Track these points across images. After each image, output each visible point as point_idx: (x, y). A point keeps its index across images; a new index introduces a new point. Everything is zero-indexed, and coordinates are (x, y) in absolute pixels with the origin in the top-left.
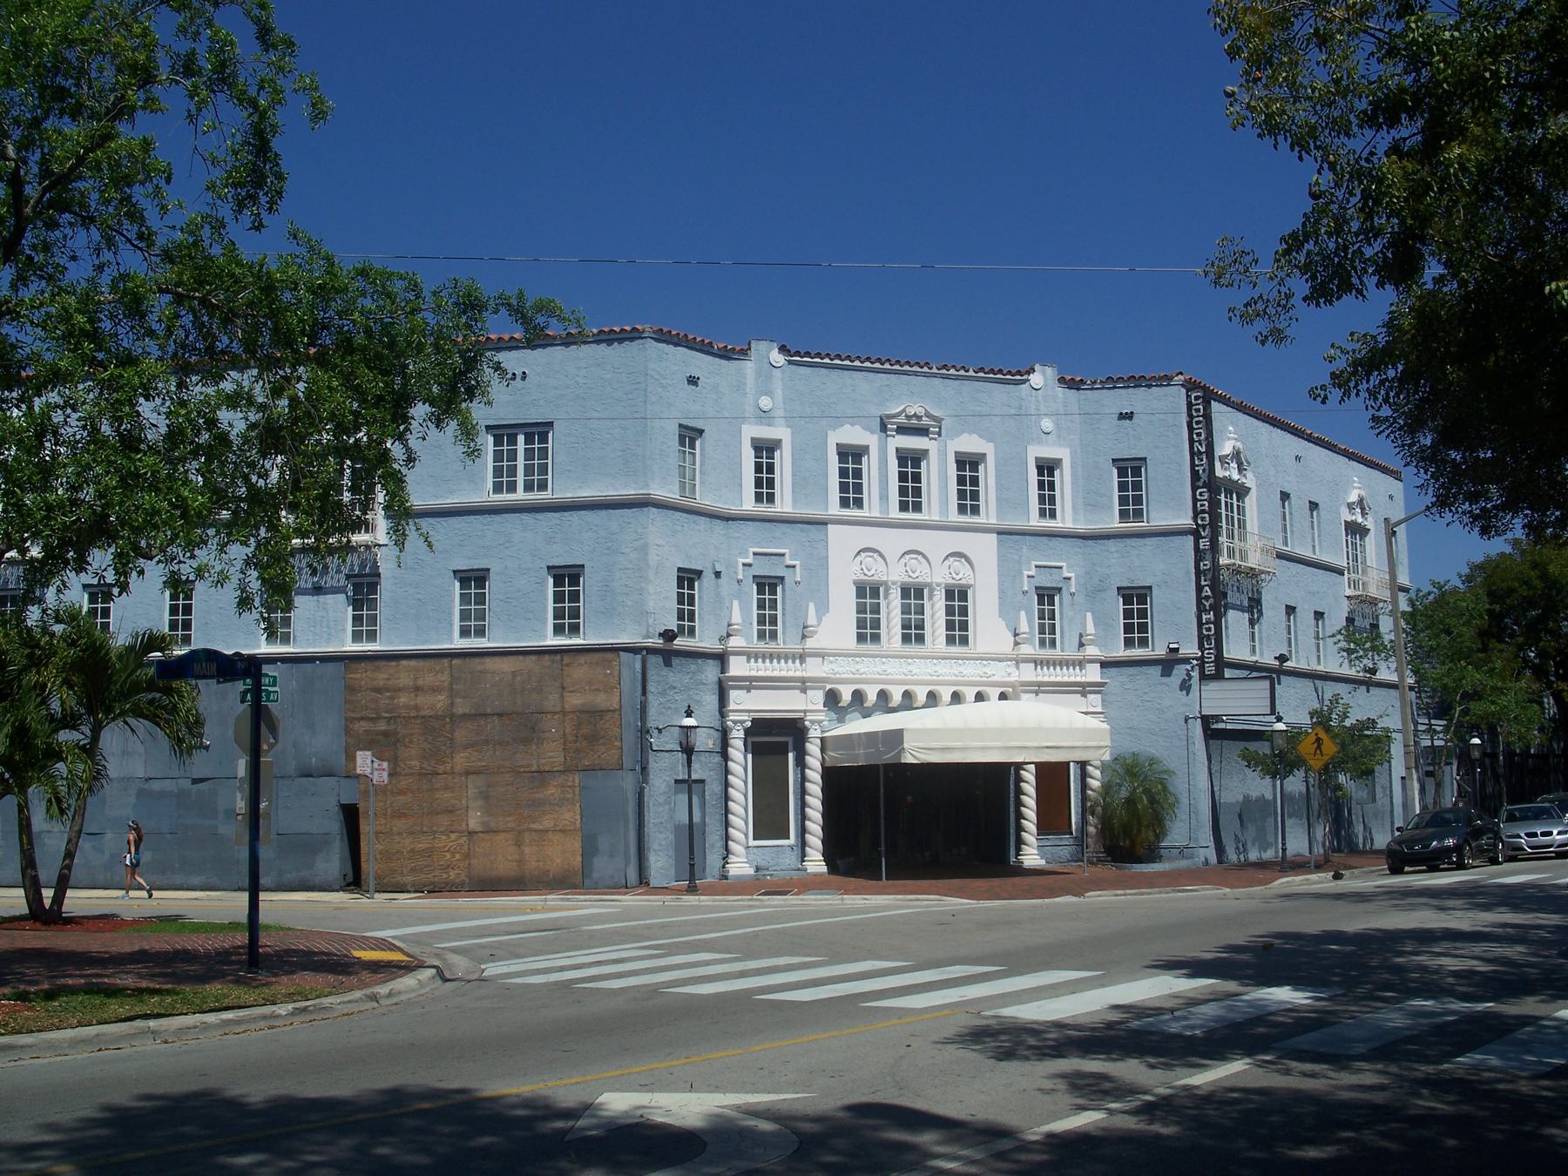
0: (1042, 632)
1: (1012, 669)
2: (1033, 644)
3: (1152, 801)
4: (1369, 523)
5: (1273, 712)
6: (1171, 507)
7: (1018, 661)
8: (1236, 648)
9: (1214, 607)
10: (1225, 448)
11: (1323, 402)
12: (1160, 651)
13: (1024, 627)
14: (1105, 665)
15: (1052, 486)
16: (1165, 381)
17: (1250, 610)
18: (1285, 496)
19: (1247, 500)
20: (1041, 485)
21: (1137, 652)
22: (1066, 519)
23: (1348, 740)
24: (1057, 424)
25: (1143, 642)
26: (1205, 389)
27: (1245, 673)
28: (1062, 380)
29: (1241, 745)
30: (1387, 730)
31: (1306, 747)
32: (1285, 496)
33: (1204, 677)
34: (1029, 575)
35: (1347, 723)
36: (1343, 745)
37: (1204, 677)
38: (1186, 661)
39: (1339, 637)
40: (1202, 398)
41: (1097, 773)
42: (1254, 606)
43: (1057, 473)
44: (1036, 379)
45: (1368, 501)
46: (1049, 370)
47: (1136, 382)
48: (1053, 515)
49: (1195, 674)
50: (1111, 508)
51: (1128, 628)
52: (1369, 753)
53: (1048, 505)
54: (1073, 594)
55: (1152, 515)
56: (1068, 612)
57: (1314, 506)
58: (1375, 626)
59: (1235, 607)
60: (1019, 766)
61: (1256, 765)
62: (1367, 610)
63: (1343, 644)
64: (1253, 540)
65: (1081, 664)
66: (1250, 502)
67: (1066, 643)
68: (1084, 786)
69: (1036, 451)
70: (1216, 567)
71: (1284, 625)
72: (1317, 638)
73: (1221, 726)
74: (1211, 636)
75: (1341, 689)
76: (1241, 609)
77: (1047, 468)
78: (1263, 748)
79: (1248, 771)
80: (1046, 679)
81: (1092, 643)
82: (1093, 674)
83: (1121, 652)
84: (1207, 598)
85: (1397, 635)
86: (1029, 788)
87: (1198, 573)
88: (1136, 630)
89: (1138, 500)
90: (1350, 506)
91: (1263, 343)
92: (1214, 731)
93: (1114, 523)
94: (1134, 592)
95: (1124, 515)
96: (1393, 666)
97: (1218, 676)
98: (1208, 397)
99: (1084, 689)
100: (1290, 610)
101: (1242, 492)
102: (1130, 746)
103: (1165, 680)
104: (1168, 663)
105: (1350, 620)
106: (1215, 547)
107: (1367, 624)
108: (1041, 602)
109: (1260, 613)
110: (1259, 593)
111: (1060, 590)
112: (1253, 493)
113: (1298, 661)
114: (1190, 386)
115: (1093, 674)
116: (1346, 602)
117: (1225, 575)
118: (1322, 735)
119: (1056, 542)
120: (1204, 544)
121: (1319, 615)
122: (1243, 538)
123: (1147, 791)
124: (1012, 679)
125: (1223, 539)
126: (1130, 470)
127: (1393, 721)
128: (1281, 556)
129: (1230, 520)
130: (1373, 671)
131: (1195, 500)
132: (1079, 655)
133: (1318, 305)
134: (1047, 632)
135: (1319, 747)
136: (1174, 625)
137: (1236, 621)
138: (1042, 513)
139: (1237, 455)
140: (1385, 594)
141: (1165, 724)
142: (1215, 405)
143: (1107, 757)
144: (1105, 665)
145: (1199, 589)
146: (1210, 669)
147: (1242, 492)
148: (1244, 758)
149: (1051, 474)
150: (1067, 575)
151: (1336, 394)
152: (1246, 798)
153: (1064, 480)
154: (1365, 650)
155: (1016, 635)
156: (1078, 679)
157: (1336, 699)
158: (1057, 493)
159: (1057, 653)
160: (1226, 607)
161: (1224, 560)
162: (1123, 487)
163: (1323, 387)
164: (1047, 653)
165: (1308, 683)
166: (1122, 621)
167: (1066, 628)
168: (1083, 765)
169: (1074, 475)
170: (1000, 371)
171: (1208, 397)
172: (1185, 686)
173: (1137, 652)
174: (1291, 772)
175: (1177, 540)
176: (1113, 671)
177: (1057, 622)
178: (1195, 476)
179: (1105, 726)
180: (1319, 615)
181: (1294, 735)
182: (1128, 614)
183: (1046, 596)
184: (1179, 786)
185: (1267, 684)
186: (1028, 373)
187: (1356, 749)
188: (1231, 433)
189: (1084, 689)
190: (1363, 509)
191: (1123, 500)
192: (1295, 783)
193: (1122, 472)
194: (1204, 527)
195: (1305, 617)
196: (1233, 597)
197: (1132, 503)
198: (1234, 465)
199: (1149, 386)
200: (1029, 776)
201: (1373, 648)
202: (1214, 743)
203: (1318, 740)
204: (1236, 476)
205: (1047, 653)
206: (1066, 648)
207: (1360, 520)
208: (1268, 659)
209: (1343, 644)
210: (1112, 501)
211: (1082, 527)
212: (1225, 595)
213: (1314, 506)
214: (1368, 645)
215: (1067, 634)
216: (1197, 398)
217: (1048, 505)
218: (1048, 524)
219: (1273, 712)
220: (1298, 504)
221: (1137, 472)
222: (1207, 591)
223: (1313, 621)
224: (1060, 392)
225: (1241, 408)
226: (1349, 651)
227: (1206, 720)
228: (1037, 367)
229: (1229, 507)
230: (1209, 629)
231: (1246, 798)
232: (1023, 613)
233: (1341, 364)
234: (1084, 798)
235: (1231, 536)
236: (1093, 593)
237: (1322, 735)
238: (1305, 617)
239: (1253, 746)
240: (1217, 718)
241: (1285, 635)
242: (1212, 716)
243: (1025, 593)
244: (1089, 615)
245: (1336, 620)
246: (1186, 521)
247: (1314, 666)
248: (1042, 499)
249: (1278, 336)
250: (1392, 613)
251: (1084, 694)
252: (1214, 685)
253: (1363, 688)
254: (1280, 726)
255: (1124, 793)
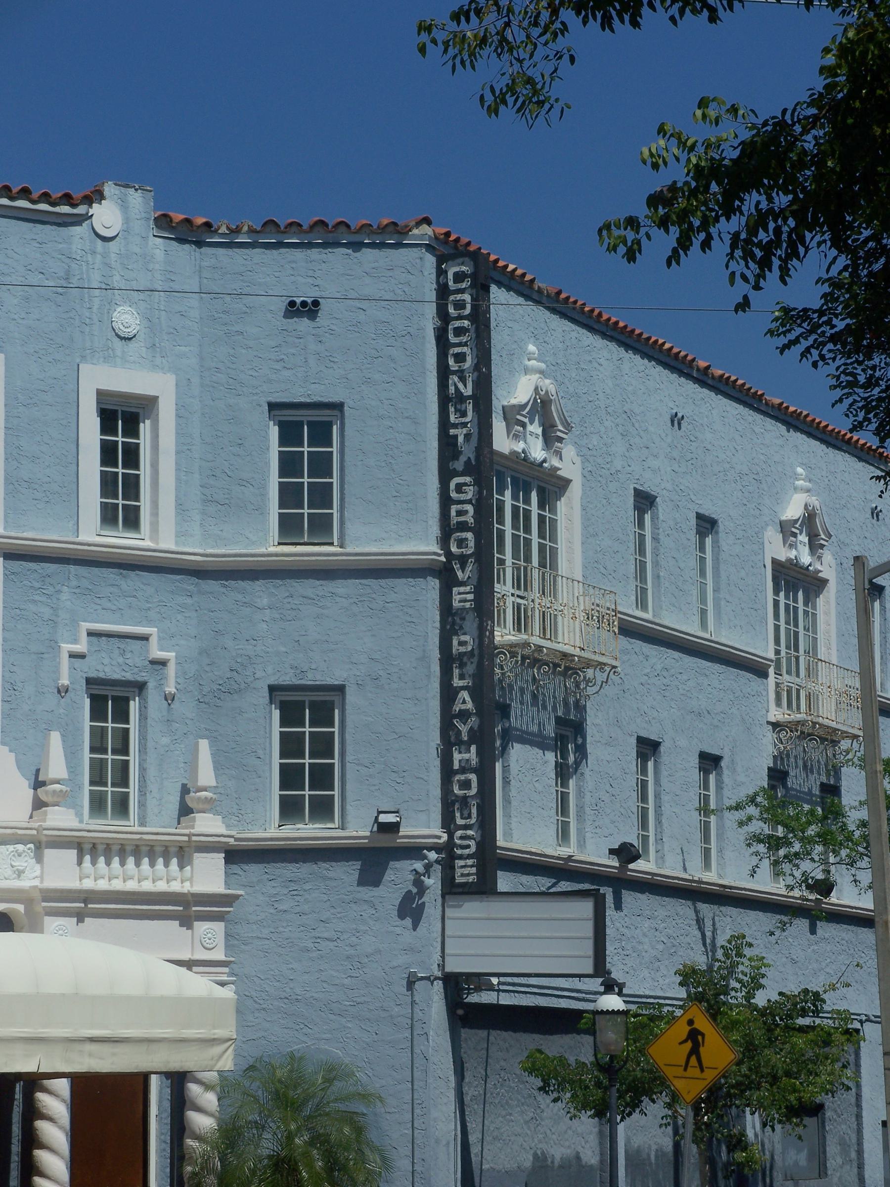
0: (98, 779)
1: (27, 862)
2: (75, 806)
3: (333, 1165)
4: (827, 567)
5: (600, 967)
6: (393, 516)
7: (41, 844)
8: (525, 829)
9: (476, 737)
10: (517, 389)
11: (631, 256)
12: (357, 828)
13: (56, 767)
14: (235, 856)
15: (132, 457)
16: (391, 235)
17: (559, 744)
18: (644, 501)
19: (562, 506)
20: (108, 453)
21: (308, 831)
22: (161, 531)
23: (759, 1034)
24: (148, 319)
25: (323, 809)
26: (476, 256)
27: (543, 883)
28: (163, 222)
29: (530, 1041)
30: (845, 1016)
31: (668, 1050)
32: (644, 501)
33: (452, 889)
34: (73, 654)
35: (760, 999)
36: (749, 1049)
37: (452, 889)
38: (414, 851)
39: (752, 810)
40: (471, 278)
41: (210, 1099)
42: (568, 737)
43: (145, 428)
44: (106, 215)
45: (825, 520)
46: (136, 198)
47: (328, 234)
48: (132, 521)
49: (433, 882)
50: (261, 510)
51: (290, 777)
52: (804, 1066)
53: (122, 497)
54: (170, 699)
55: (352, 529)
56: (159, 738)
57: (706, 525)
58: (831, 790)
59: (526, 739)
60: (33, 1082)
61: (561, 1087)
62: (816, 753)
63: (758, 827)
64: (569, 592)
65: (182, 852)
66: (569, 511)
67: (151, 803)
68: (179, 1128)
69: (100, 377)
70: (486, 649)
71: (632, 781)
72: (704, 809)
73: (486, 998)
74: (471, 800)
75: (755, 924)
76: (538, 741)
77: (122, 417)
78: (577, 1050)
79: (545, 1100)
80: (103, 885)
81: (210, 806)
82: (208, 876)
83: (269, 828)
84: (464, 715)
85: (874, 811)
86: (55, 1134)
87: (448, 660)
88: (308, 781)
89: (322, 496)
90: (787, 530)
91: (494, 111)
92: (472, 1012)
93: (266, 543)
94: (307, 697)
95: (289, 527)
96: (865, 877)
97: (483, 888)
98: (485, 275)
99: (186, 909)
100: (648, 748)
101: (551, 487)
102: (282, 1038)
103: (367, 893)
104: (375, 856)
105: (777, 775)
106: (484, 605)
107: (813, 784)
108: (98, 713)
109: (581, 751)
110: (580, 708)
111: (140, 687)
112: (575, 491)
113: (661, 859)
114: (446, 250)
115: (208, 876)
116: (769, 736)
117: (504, 669)
118: (703, 1024)
119: (135, 581)
120: (462, 597)
121: (710, 762)
122: (549, 588)
123: (318, 1140)
124: (25, 883)
125: (504, 588)
126: (307, 428)
127: (860, 999)
128: (630, 630)
129: (522, 549)
130: (825, 887)
131: (446, 501)
132: (175, 833)
133: (607, 23)
134: (110, 781)
135: (695, 1051)
136: (392, 777)
137: (526, 770)
138: (109, 516)
139: (541, 407)
140: (850, 721)
141: (366, 988)
142: (497, 294)
143: (227, 1063)
144: (235, 856)
145: (448, 694)
146: (466, 871)
147: (551, 487)
148: (532, 1070)
149: (132, 428)
150: (157, 653)
151: (664, 241)
152: (541, 1162)
153: (161, 445)
154: (807, 841)
155: (38, 784)
156: (176, 887)
157: (739, 943)
158: (145, 472)
159: (130, 827)
160: (507, 737)
161: (504, 635)
162: (289, 465)
163: (632, 222)
164: (107, 827)
165: (683, 909)
166: (276, 761)
167: (152, 772)
168: (178, 1080)
169: (181, 433)
170: (25, 193)
171: (485, 275)
172: (410, 909)
173: (308, 831)
174: (635, 1105)
175: (403, 587)
176: (254, 871)
177: (133, 758)
178: (448, 446)
179: (228, 993)
180: (710, 762)
181: (643, 1022)
182: (290, 746)
183: (110, 699)
184: (390, 1129)
185: (586, 907)
186: (89, 200)
187: (775, 1058)
188: (531, 358)
189: (186, 909)
190: (813, 537)
191: (289, 495)
192: (646, 1130)
193: (289, 434)
194: (463, 560)
195: (679, 765)
196: (522, 717)
197: (308, 501)
198: (535, 428)
199: (357, 246)
200: (56, 1104)
201: (825, 838)
202: (472, 1037)
203: (694, 1036)
204: (537, 452)
205: (107, 827)
206: (151, 818)
207: (806, 559)
208: (596, 853)
209: (758, 827)
210: (264, 495)
211: (197, 549)
212: (504, 710)
213: (706, 525)
214: (812, 830)
215: (153, 787)
216: (459, 277)
217: (122, 497)
218: (119, 540)
219: (600, 967)
220: (673, 519)
221: (321, 434)
222: (465, 701)
223: (695, 775)
224: (159, 247)
225: (561, 306)
226: (774, 843)
227: (455, 985)
228: (109, 189)
229: (521, 519)
230: (466, 785)
231: (541, 1162)
232: (55, 738)
233: (678, 173)
234: (177, 1155)
235: (499, 582)
236: (215, 697)
237: (703, 1024)
238: (679, 765)
239: (556, 1046)
240: (479, 981)
241: (633, 803)
242: (469, 976)
243: (63, 691)
244: (204, 746)
245: (748, 773)
246: (425, 545)
247: (696, 872)
248: (108, 484)
249: (526, 96)
250: (865, 763)
251: (186, 921)
252: (474, 907)
253: (802, 924)
254: (612, 1002)
255: (268, 1145)
